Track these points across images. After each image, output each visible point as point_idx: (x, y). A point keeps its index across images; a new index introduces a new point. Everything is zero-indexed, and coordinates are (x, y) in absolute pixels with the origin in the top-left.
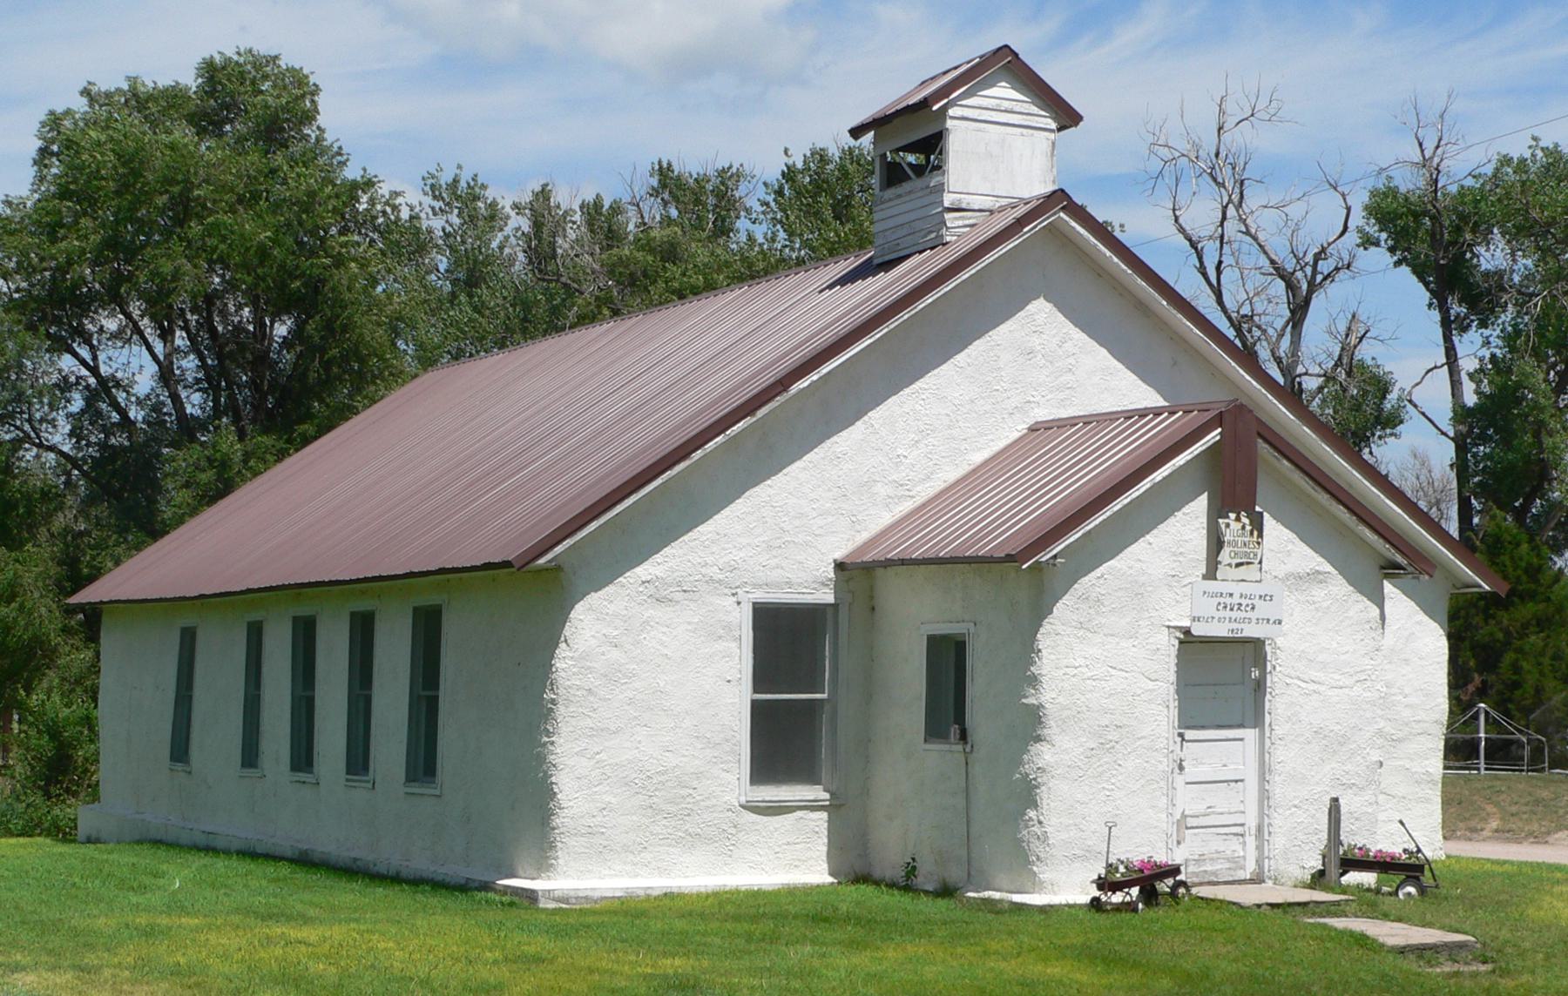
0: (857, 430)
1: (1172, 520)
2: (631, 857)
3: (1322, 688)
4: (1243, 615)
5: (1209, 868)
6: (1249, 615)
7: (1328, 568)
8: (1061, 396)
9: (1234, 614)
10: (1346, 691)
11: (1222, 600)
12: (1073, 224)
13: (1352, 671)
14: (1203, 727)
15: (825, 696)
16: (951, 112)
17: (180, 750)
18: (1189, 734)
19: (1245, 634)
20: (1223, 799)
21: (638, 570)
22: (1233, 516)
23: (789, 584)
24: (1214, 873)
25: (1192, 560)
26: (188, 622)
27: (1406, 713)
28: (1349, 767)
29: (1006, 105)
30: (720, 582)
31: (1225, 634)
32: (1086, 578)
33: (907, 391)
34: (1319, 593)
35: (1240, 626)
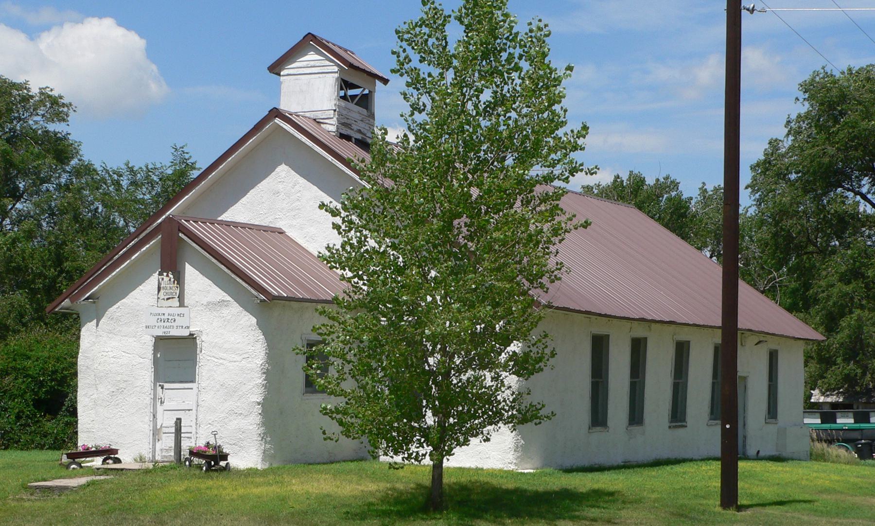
3: (225, 362)
4: (170, 324)
6: (173, 324)
7: (229, 298)
8: (293, 213)
18: (166, 386)
22: (165, 274)
26: (774, 347)
29: (312, 63)
34: (225, 311)
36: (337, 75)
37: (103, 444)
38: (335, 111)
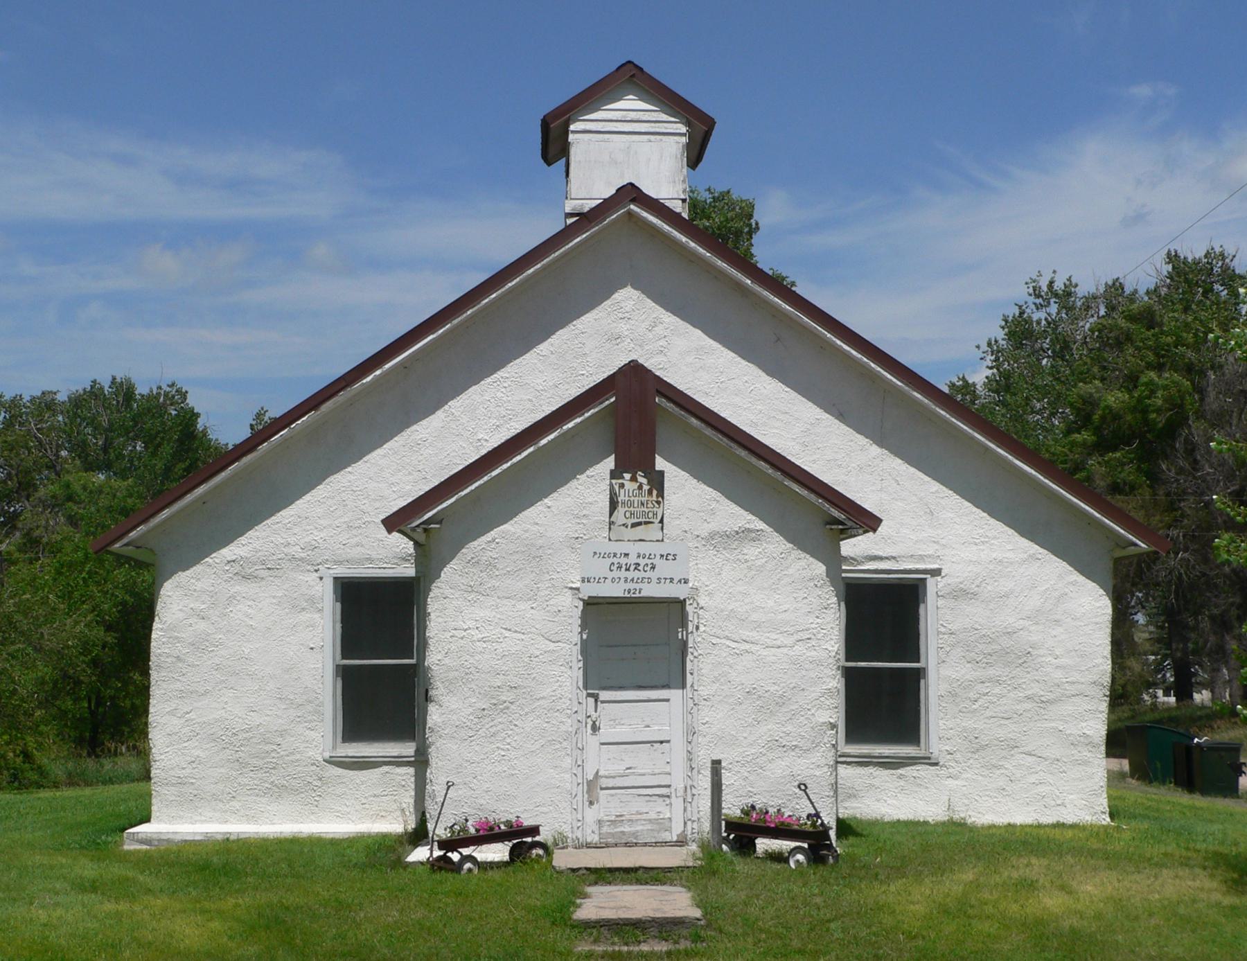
0: (437, 420)
1: (574, 483)
2: (221, 805)
3: (754, 648)
4: (642, 574)
5: (627, 829)
7: (761, 525)
9: (630, 575)
10: (785, 650)
11: (616, 560)
12: (645, 214)
13: (791, 630)
14: (621, 688)
15: (413, 661)
16: (572, 127)
17: (668, 700)
18: (604, 695)
19: (643, 594)
20: (645, 763)
21: (224, 551)
22: (627, 476)
23: (370, 560)
24: (635, 834)
25: (597, 522)
27: (1058, 674)
28: (789, 728)
29: (632, 115)
30: (301, 559)
31: (621, 595)
32: (475, 543)
33: (489, 380)
34: (751, 551)
35: (638, 586)
36: (684, 140)
37: (504, 812)
38: (684, 201)
